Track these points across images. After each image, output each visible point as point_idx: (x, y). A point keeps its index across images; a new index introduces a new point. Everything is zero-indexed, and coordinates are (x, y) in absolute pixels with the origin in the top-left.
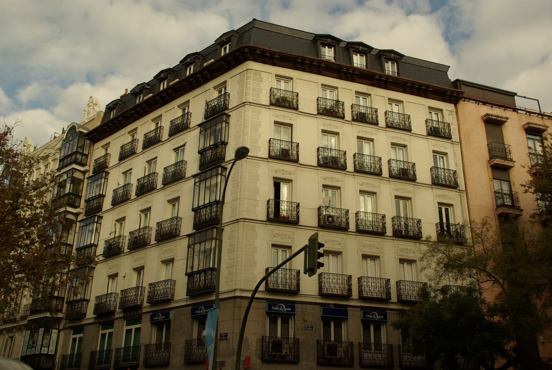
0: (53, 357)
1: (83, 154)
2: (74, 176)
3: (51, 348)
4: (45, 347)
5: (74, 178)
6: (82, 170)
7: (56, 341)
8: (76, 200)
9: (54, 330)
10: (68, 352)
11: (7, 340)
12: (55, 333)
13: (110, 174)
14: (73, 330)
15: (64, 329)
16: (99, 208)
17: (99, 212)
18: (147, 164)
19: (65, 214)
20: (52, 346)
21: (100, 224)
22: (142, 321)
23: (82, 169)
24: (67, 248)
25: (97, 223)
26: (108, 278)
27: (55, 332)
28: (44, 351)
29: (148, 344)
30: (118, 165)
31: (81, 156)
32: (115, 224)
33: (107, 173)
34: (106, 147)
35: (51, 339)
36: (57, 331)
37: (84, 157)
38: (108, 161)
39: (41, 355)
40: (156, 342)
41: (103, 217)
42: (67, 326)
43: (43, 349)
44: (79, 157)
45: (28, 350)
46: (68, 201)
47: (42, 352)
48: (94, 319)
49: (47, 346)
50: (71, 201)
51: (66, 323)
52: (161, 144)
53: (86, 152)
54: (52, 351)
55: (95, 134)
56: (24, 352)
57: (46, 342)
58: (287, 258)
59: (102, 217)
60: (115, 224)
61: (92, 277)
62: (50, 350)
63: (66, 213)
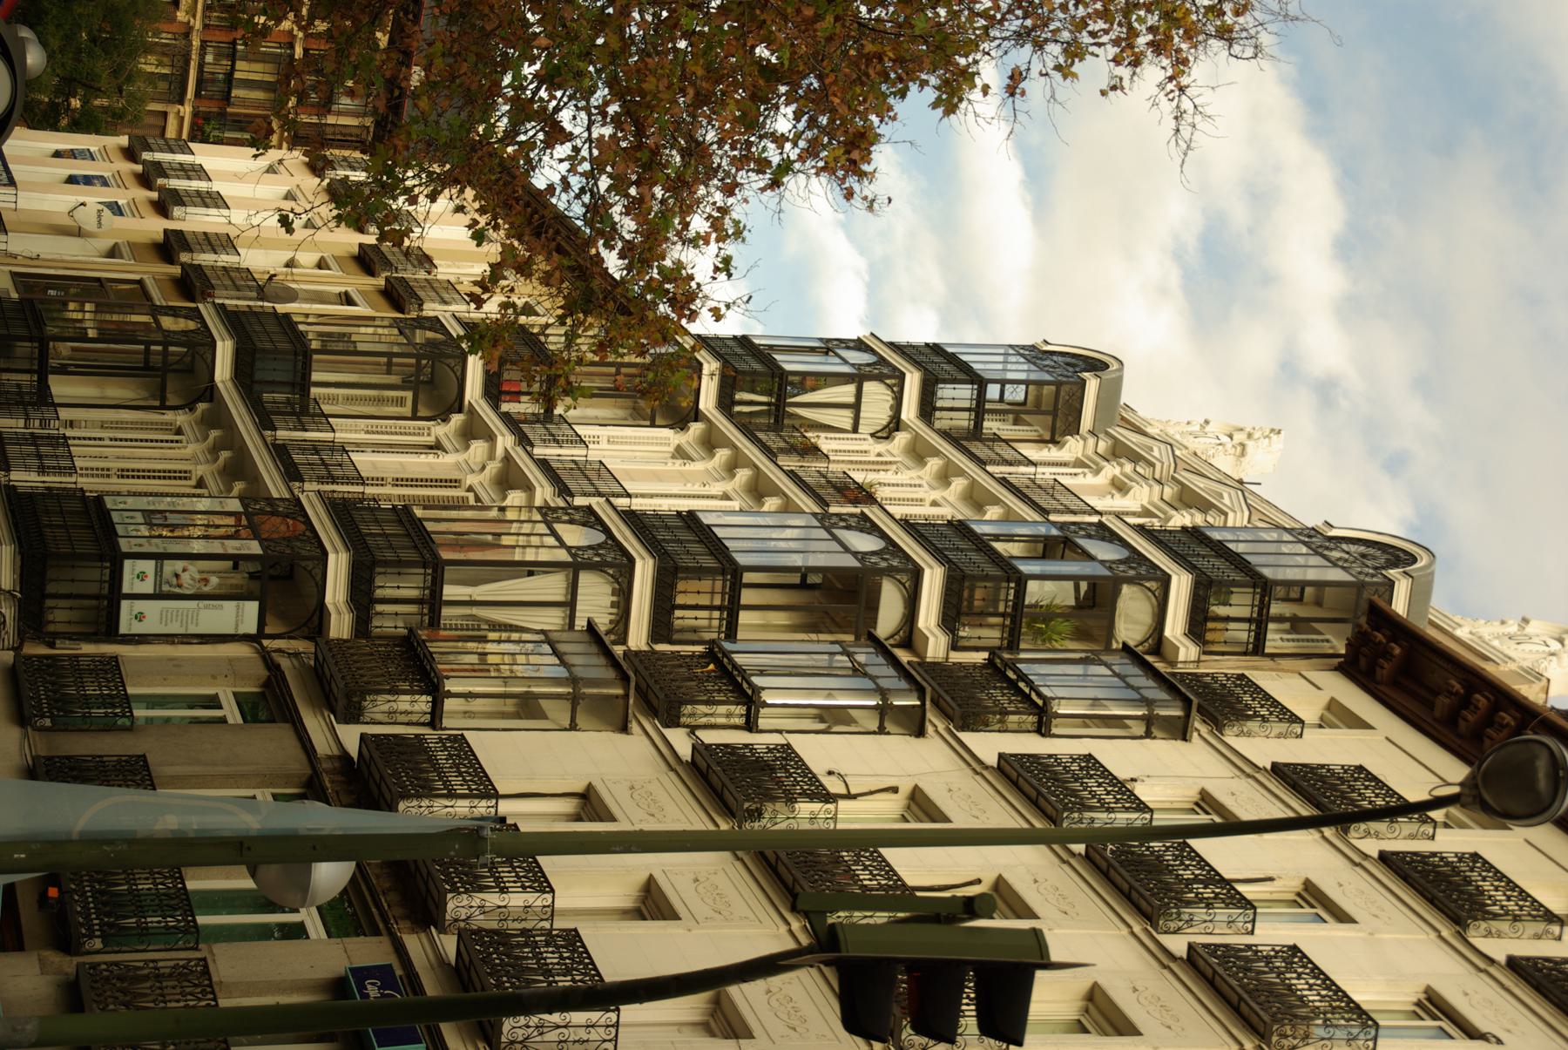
0: (108, 630)
1: (1259, 623)
2: (1125, 589)
3: (152, 608)
4: (159, 572)
5: (1116, 593)
6: (1167, 633)
7: (192, 630)
8: (991, 626)
9: (252, 608)
10: (134, 685)
11: (184, 475)
12: (239, 619)
13: (1179, 743)
14: (262, 694)
15: (266, 657)
16: (969, 717)
17: (946, 715)
18: (1297, 885)
19: (897, 570)
20: (164, 617)
21: (882, 730)
22: (346, 940)
23: (1175, 626)
24: (716, 614)
25: (883, 711)
26: (579, 787)
27: (246, 616)
28: (137, 576)
29: (215, 979)
30: (1248, 770)
31: (1245, 612)
32: (895, 790)
33: (1181, 731)
34: (1338, 716)
35: (203, 603)
36: (251, 627)
37: (1241, 633)
38: (1253, 725)
39: (116, 560)
40: (206, 926)
41: (921, 740)
42: (285, 663)
43: (148, 566)
44: (1240, 605)
45: (139, 515)
46: (975, 578)
47: (127, 564)
48: (336, 752)
49: (166, 588)
50: (979, 594)
51: (296, 655)
52: (1445, 933)
53: (1276, 639)
54: (140, 617)
55: (1397, 651)
56: (132, 518)
57: (185, 577)
58: (884, 662)
59: (920, 732)
60: (895, 790)
61: (573, 727)
62: (140, 605)
63: (904, 578)
